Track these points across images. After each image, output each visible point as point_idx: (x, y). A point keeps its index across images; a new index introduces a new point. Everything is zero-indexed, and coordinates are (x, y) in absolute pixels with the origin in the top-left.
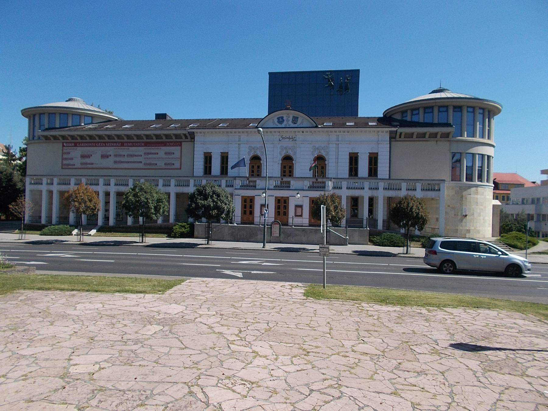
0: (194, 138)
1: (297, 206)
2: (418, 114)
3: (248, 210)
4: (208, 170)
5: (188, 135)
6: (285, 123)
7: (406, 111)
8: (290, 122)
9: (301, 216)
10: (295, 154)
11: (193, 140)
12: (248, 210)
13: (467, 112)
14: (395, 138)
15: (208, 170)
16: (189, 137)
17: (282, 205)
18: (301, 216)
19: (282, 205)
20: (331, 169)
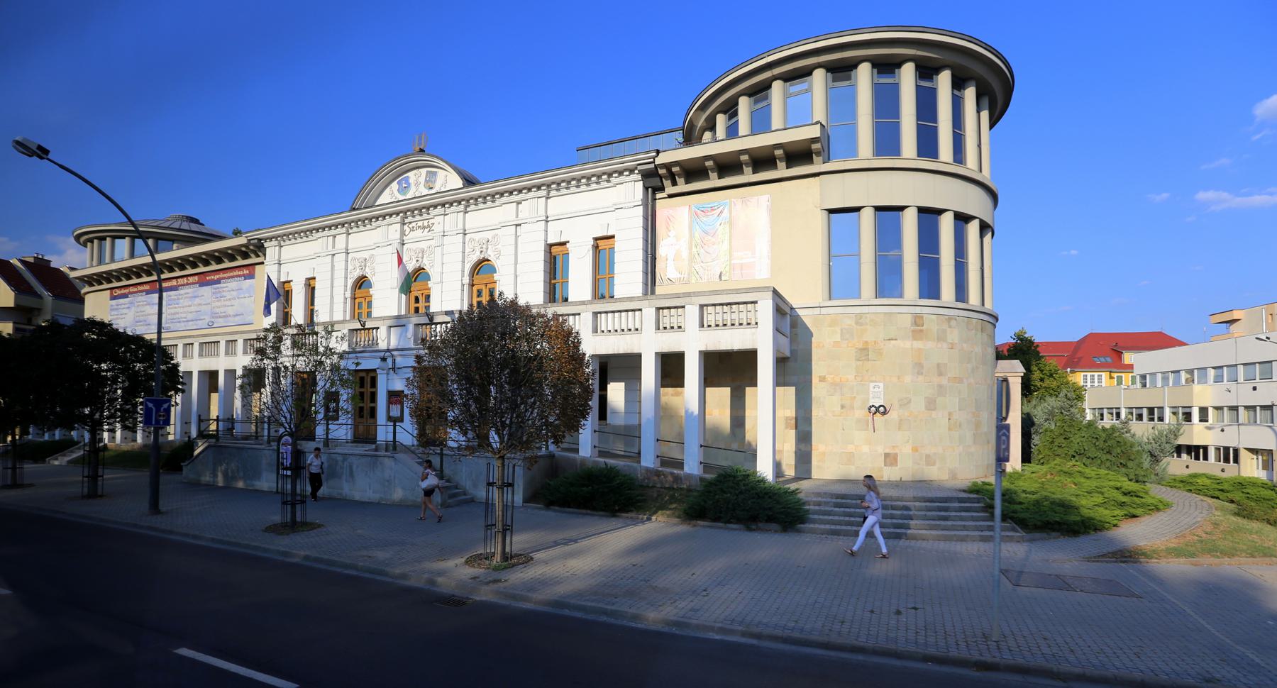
6: (413, 189)
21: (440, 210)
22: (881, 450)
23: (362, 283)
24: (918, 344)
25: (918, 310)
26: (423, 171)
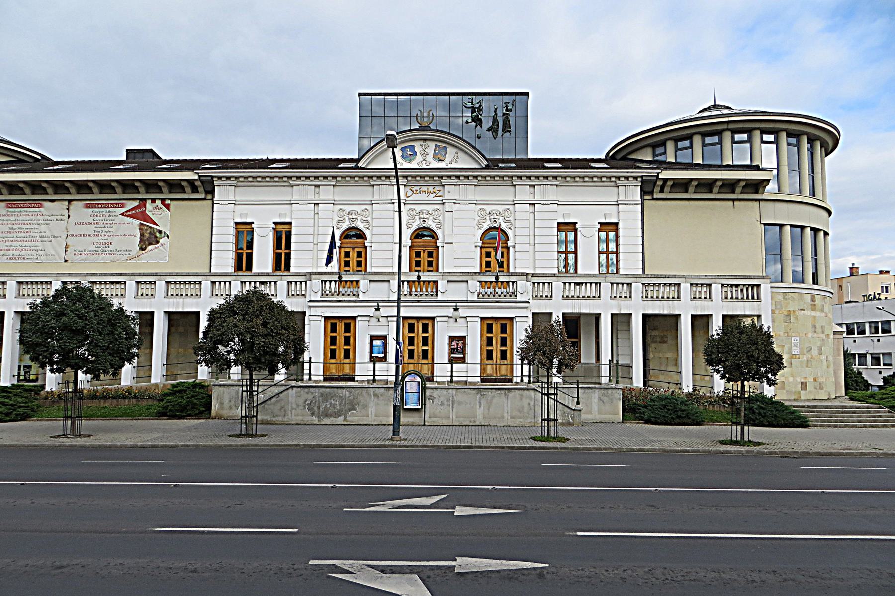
0: (212, 192)
1: (384, 360)
2: (691, 147)
3: (497, 348)
4: (244, 262)
5: (198, 184)
6: (419, 157)
7: (663, 144)
8: (430, 158)
9: (373, 338)
10: (441, 225)
11: (209, 197)
12: (497, 348)
13: (788, 144)
14: (651, 193)
15: (244, 262)
16: (201, 189)
17: (417, 332)
18: (373, 338)
19: (417, 332)
20: (518, 262)
21: (454, 181)
22: (799, 380)
23: (355, 235)
24: (814, 313)
25: (813, 292)
26: (432, 145)
